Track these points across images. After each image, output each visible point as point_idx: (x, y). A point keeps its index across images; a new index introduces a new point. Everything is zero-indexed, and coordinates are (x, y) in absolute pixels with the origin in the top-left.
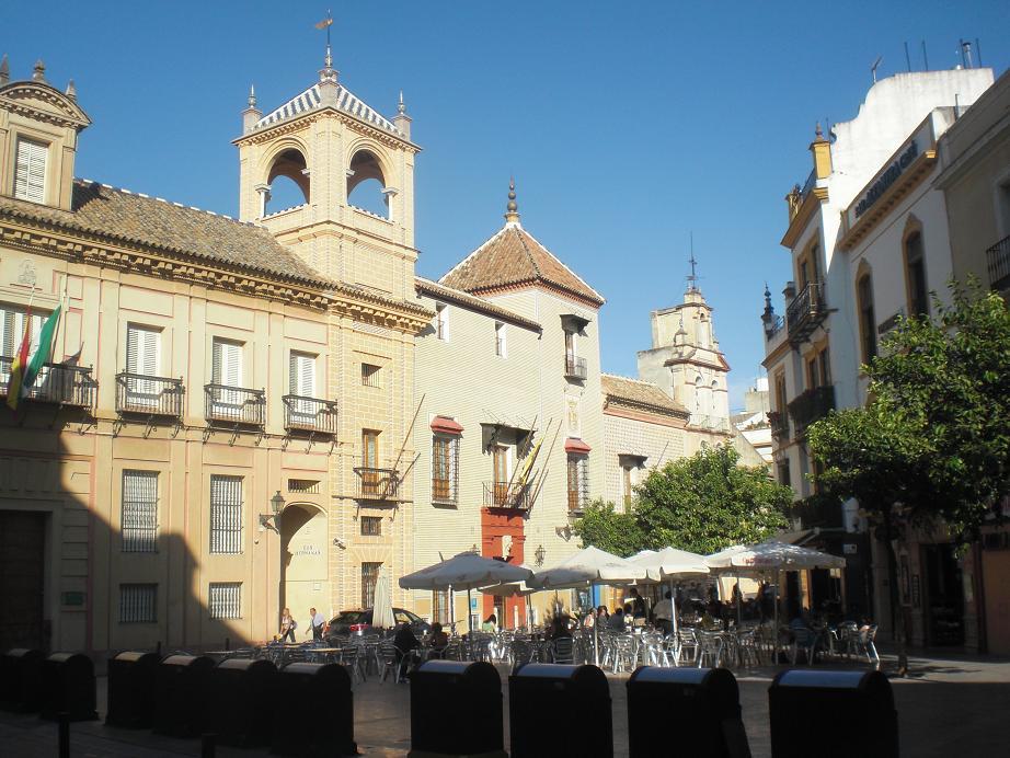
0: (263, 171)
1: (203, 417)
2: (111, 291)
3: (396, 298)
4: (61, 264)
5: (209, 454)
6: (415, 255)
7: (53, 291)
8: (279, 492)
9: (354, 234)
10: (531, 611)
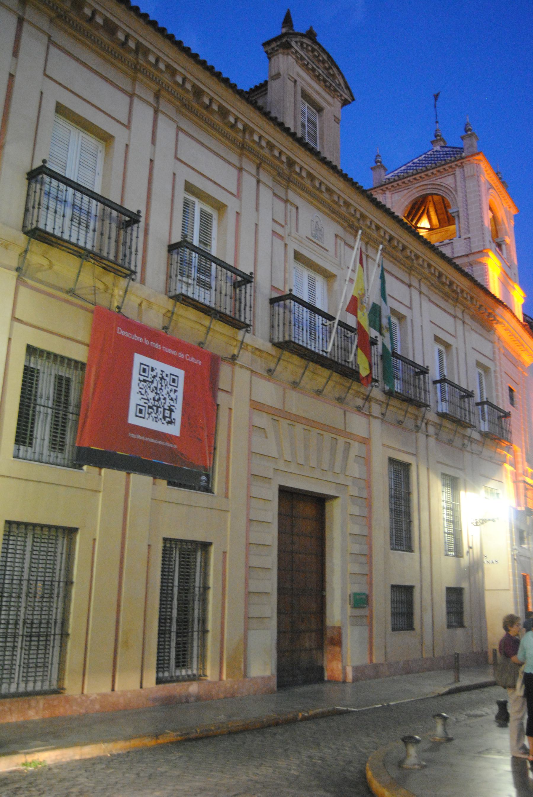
0: (406, 203)
2: (166, 130)
8: (44, 161)
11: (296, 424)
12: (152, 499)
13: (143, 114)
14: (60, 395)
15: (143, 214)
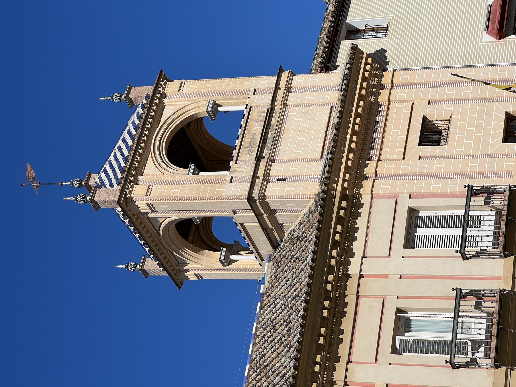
1: (493, 370)
3: (334, 97)
6: (285, 76)
9: (263, 164)
10: (178, 183)
11: (335, 78)
13: (381, 187)
15: (147, 202)
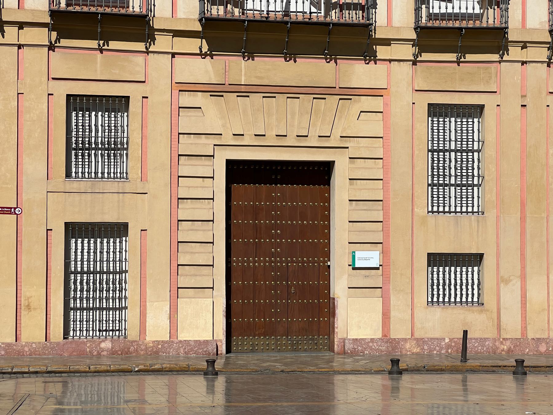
4: (519, 194)
5: (424, 77)
7: (53, 79)
12: (436, 111)
14: (113, 252)
